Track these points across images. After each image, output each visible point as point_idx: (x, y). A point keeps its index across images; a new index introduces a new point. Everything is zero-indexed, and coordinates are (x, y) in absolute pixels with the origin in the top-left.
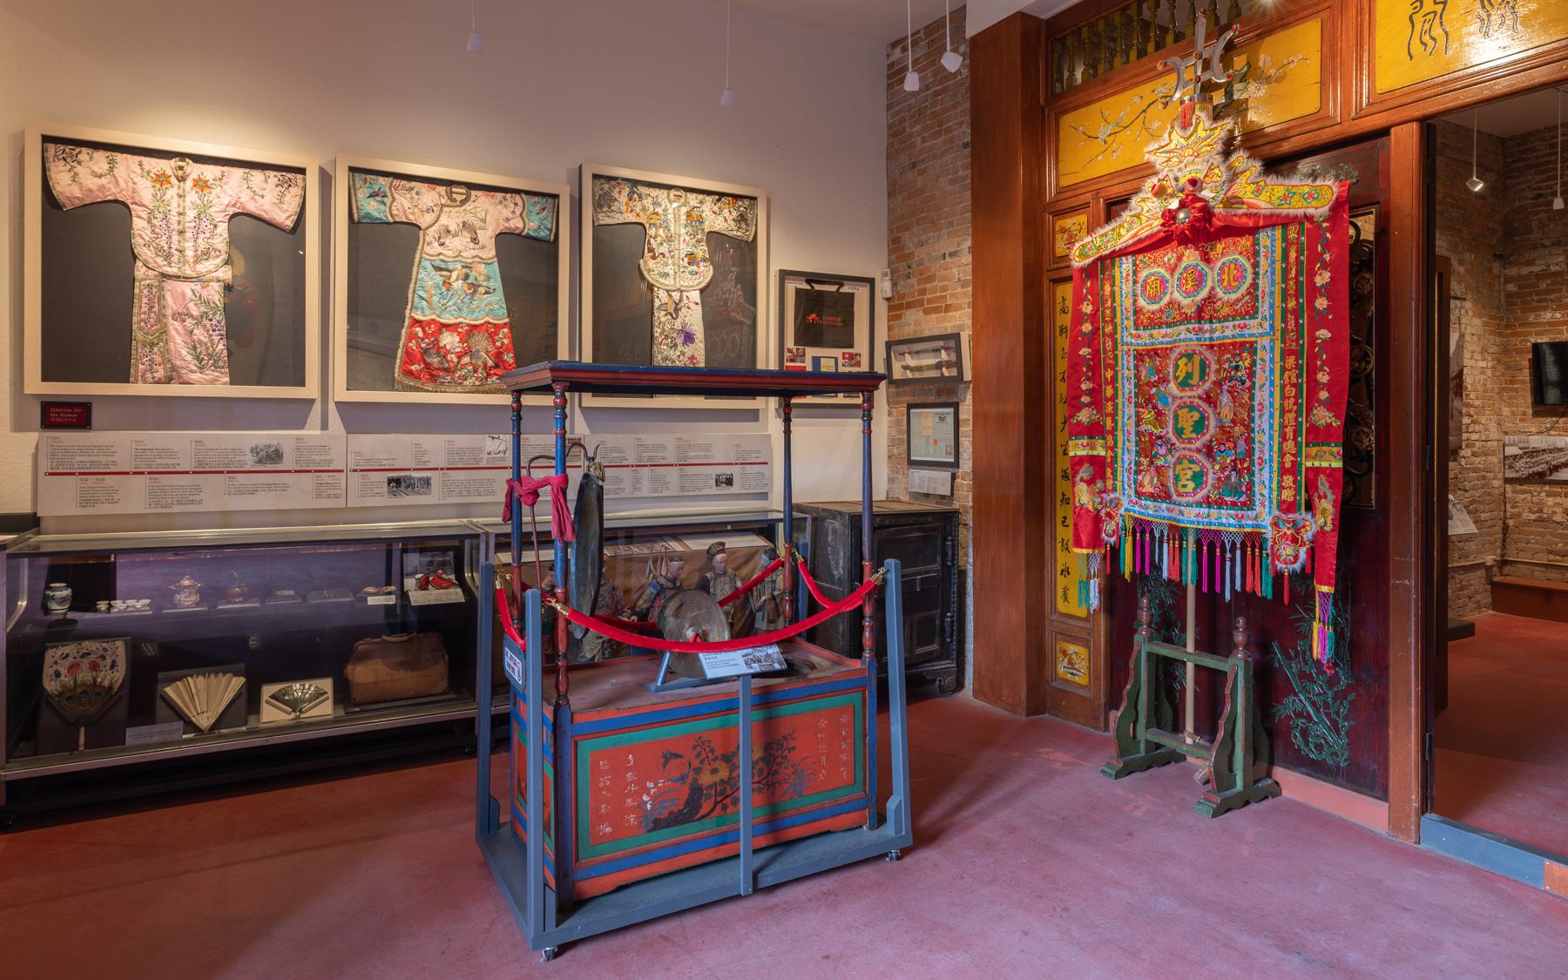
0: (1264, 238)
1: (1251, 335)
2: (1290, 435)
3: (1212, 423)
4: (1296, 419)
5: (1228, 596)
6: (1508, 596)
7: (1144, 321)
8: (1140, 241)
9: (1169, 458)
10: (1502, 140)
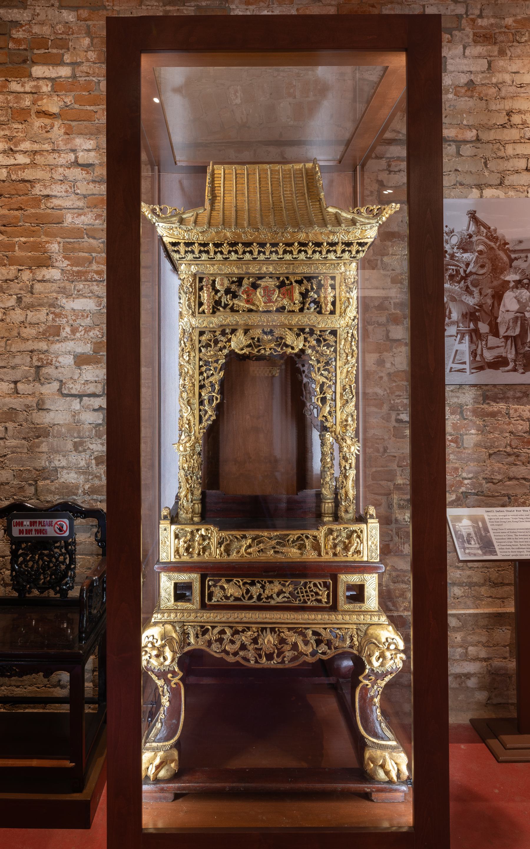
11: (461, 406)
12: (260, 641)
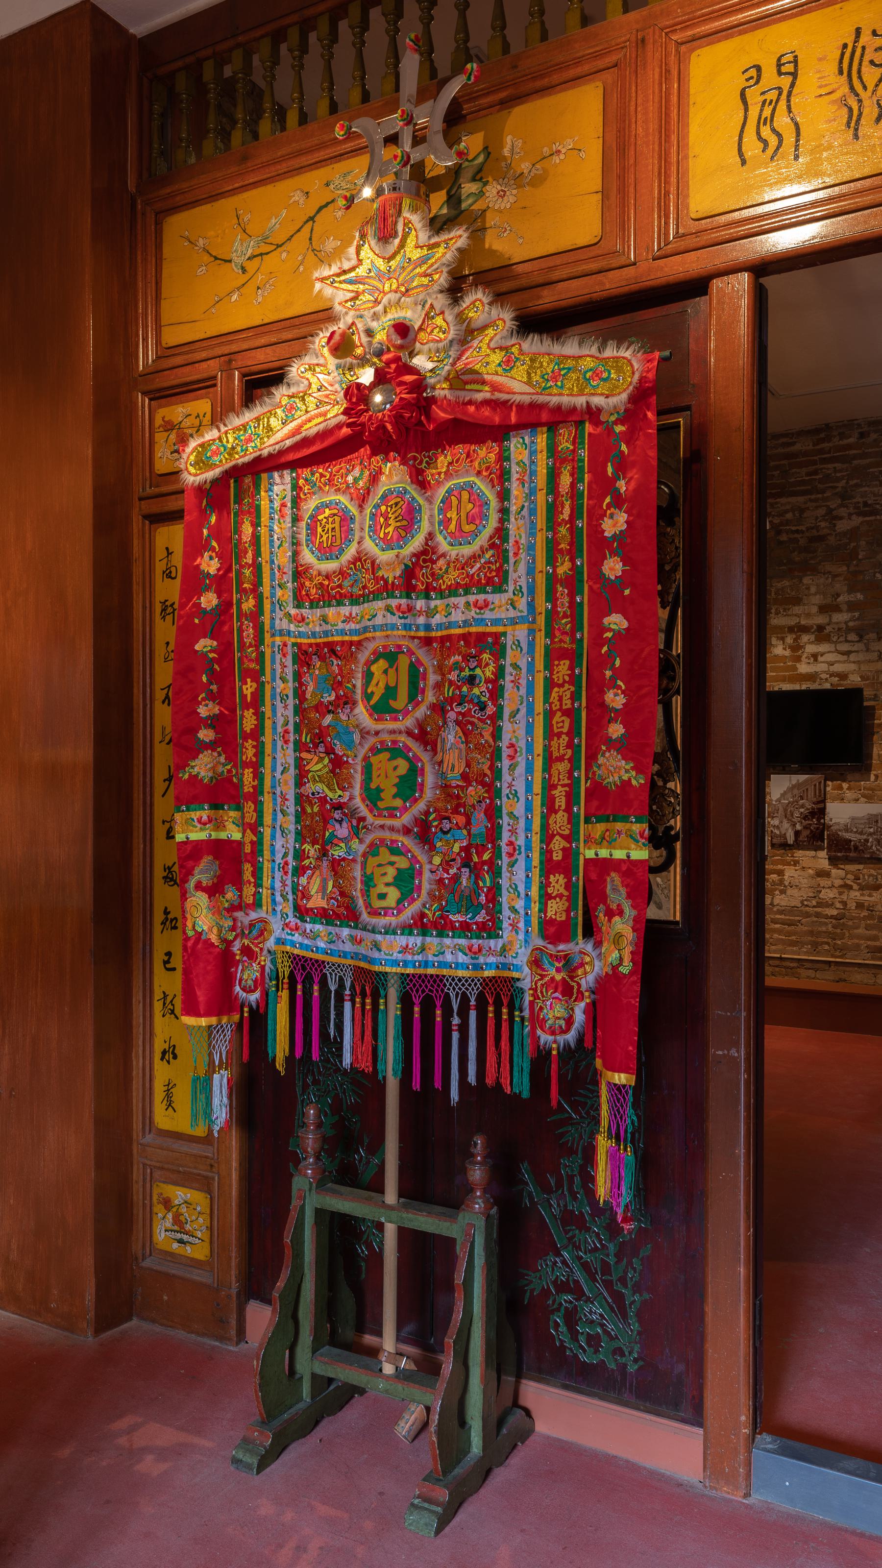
0: (518, 447)
1: (496, 622)
2: (561, 802)
3: (429, 779)
4: (570, 773)
5: (454, 1095)
7: (312, 592)
8: (306, 442)
9: (355, 844)
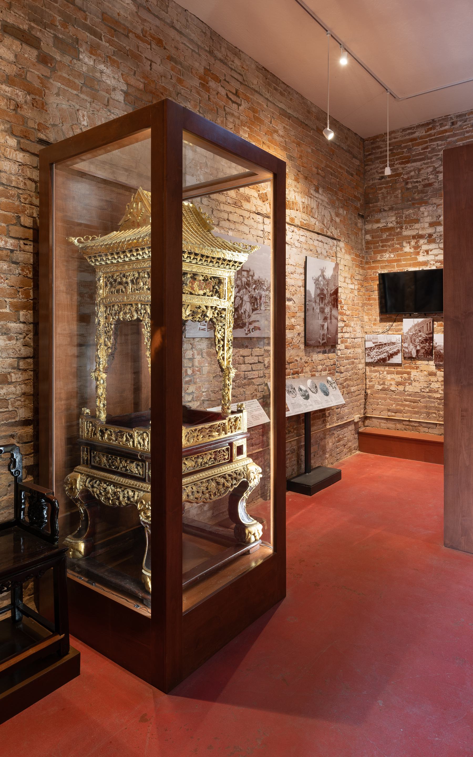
6: (371, 442)
10: (363, 140)
11: (201, 350)
12: (209, 487)
